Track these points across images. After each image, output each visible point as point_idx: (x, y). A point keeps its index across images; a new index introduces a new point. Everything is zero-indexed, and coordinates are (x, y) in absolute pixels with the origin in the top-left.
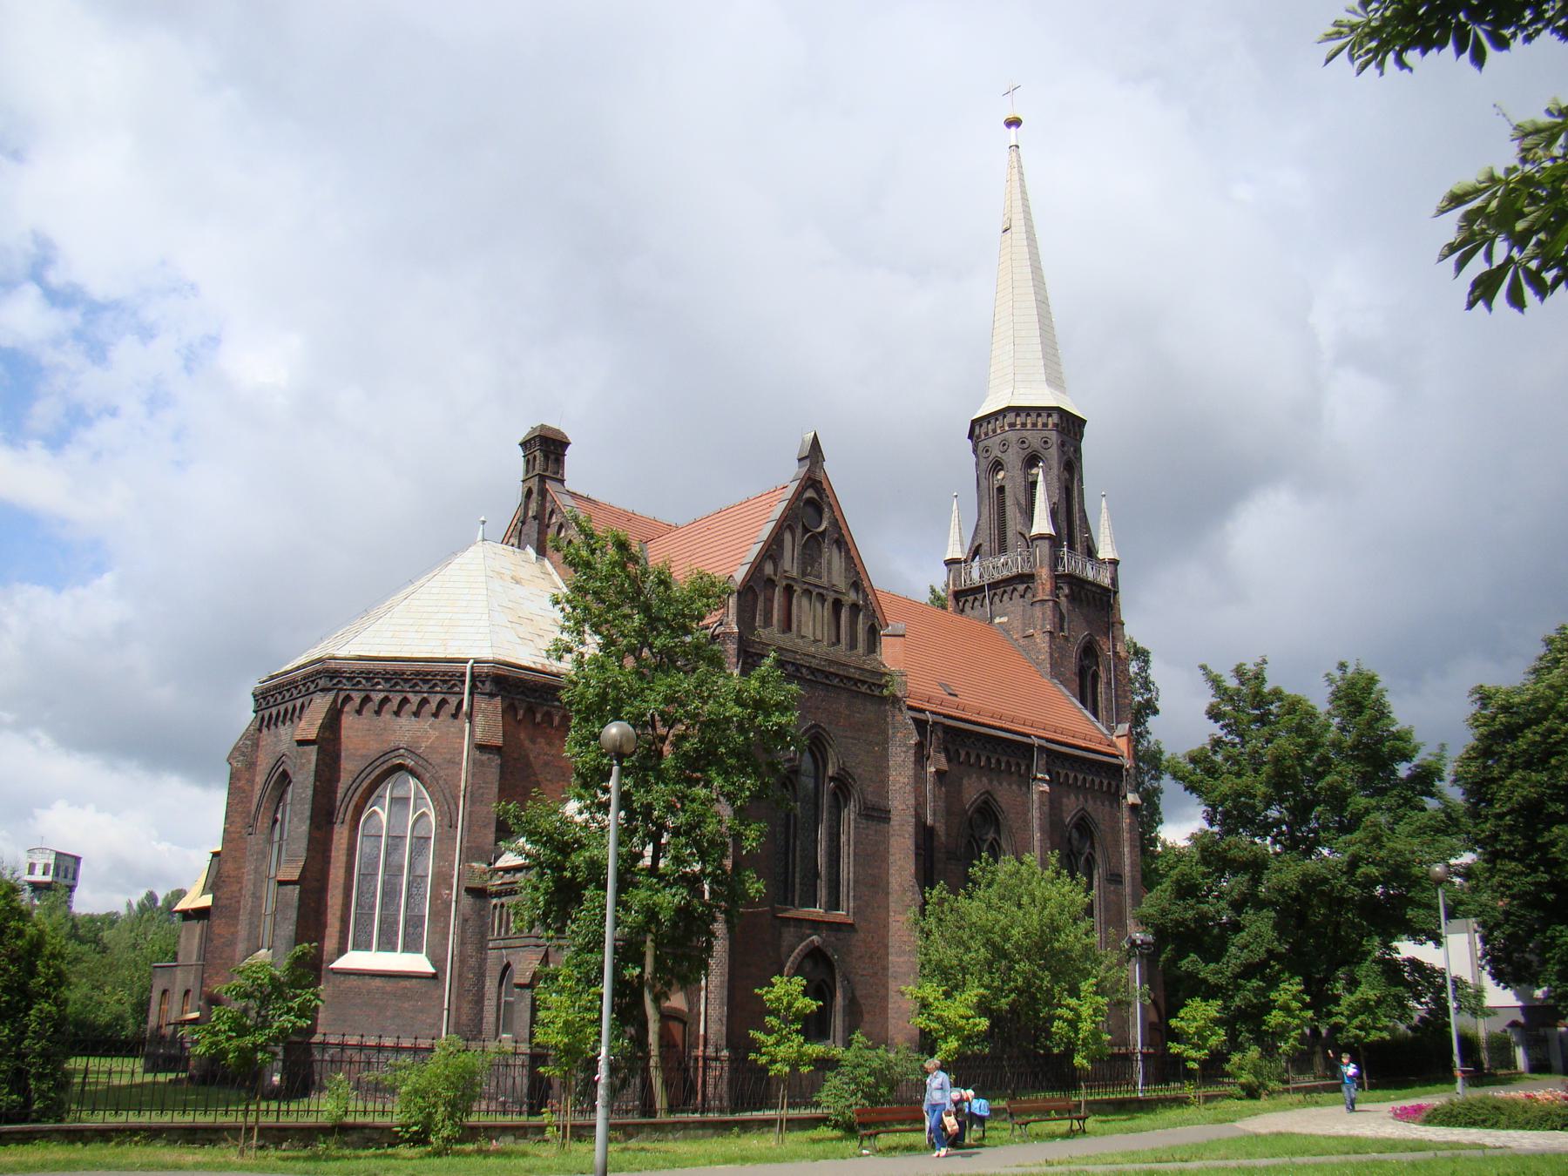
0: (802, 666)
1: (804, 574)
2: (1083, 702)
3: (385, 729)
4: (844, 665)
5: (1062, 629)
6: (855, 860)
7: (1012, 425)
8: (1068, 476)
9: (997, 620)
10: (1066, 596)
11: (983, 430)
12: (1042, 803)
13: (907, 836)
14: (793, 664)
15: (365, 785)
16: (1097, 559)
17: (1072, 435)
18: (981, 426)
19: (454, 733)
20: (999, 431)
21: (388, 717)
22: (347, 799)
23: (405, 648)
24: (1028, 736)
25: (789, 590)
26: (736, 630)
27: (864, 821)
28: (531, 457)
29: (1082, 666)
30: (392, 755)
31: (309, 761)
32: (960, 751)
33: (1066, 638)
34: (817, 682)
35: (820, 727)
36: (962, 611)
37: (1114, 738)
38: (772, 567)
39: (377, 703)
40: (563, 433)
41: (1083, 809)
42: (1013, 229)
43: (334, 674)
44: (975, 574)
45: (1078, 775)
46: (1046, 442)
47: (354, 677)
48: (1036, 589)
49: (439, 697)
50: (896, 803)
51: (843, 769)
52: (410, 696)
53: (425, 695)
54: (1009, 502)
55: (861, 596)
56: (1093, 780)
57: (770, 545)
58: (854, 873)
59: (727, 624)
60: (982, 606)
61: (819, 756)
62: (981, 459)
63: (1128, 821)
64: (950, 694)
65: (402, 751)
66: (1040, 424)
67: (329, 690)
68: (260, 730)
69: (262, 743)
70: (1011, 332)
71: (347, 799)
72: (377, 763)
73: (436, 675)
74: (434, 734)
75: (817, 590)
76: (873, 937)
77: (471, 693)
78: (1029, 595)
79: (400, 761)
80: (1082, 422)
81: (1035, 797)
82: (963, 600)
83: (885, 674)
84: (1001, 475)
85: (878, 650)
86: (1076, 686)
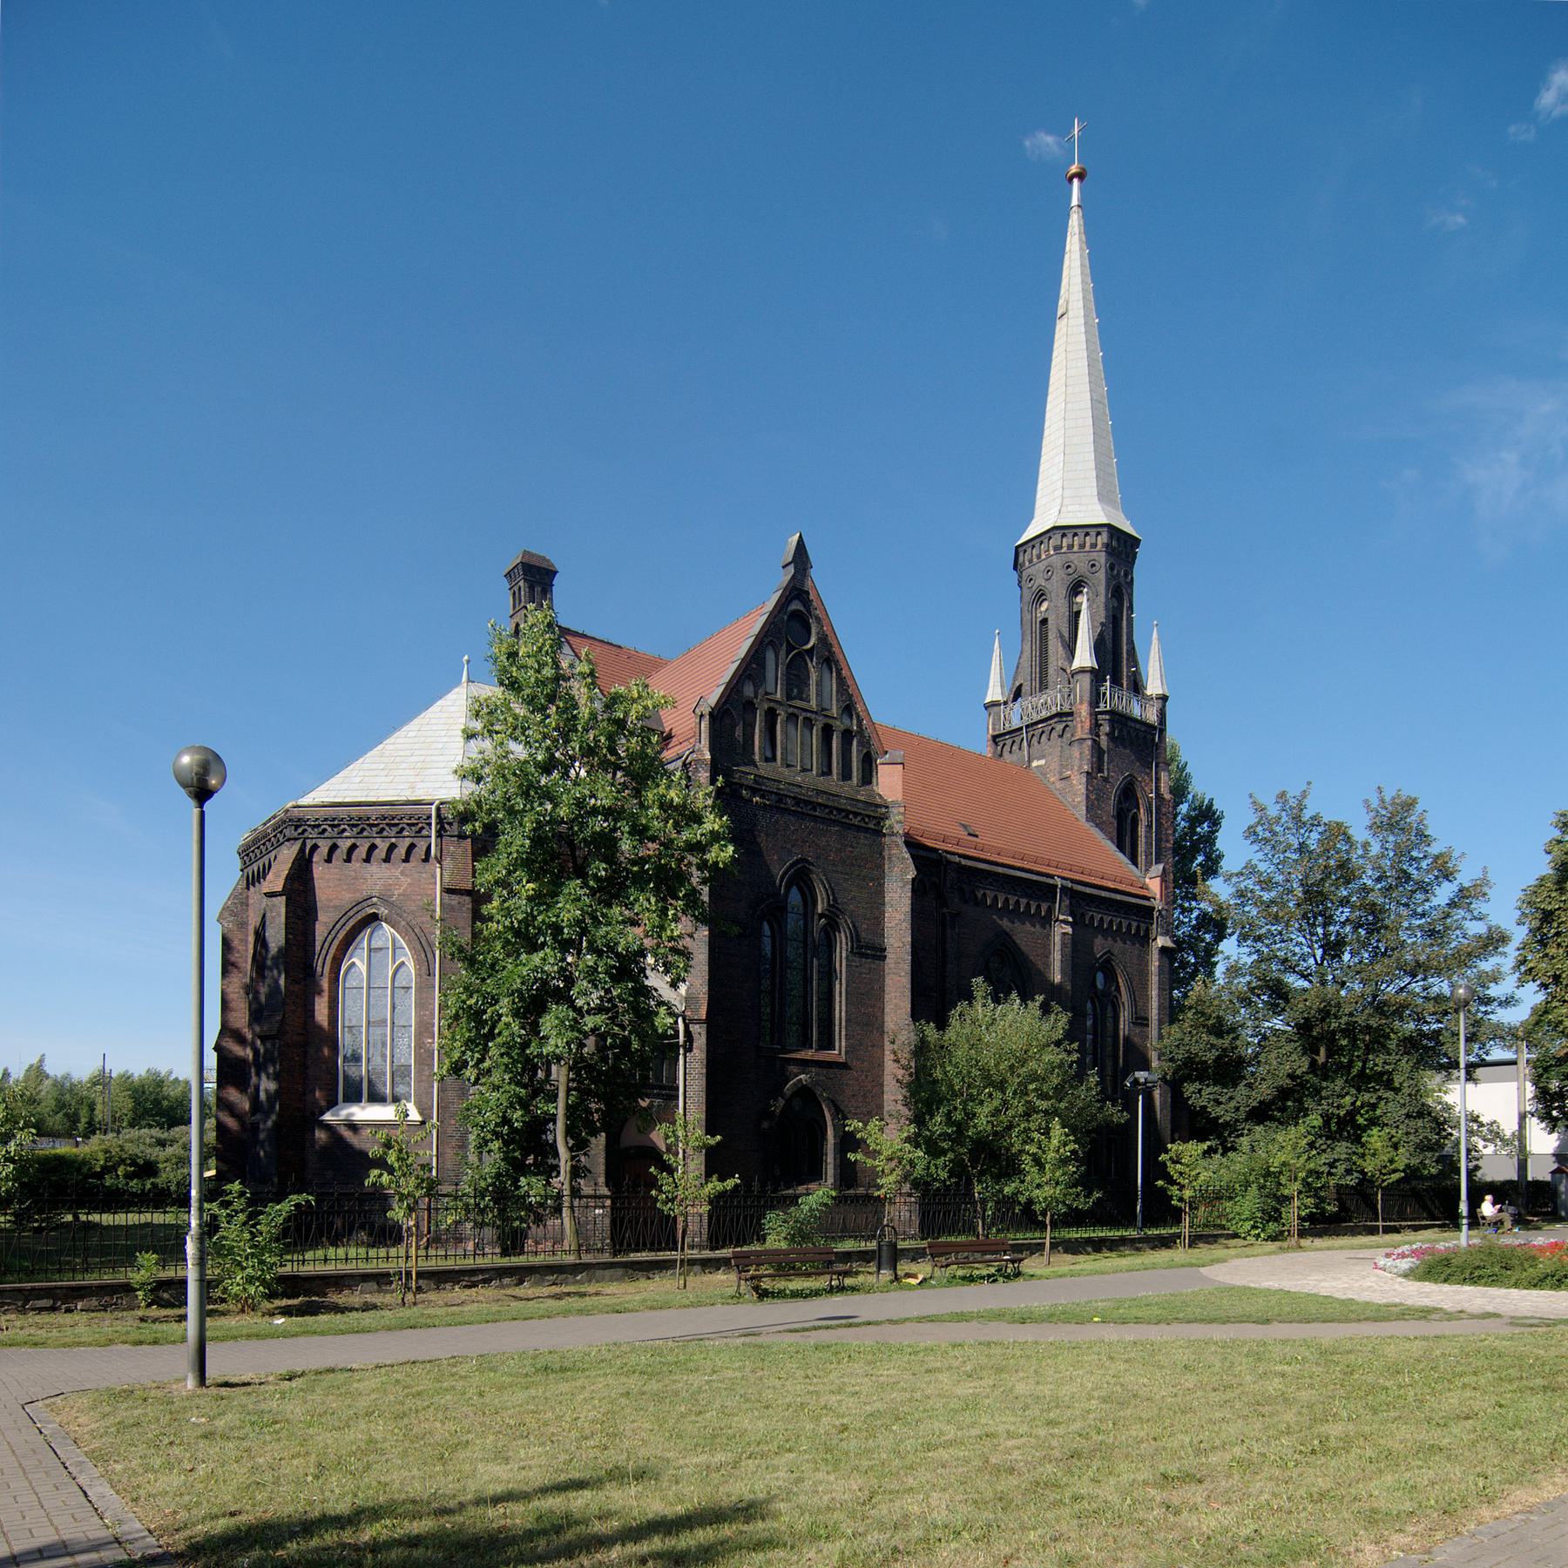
0: (786, 796)
1: (789, 697)
2: (1121, 847)
3: (356, 878)
4: (834, 795)
5: (1100, 770)
6: (847, 998)
7: (1058, 548)
8: (1116, 605)
9: (1035, 764)
10: (1107, 734)
11: (1027, 556)
12: (1063, 944)
13: (903, 974)
14: (776, 794)
15: (341, 936)
16: (1143, 694)
17: (1124, 556)
18: (1025, 551)
19: (425, 879)
20: (1043, 557)
21: (358, 865)
22: (324, 952)
23: (372, 793)
24: (1052, 877)
25: (771, 716)
26: (708, 756)
27: (857, 959)
28: (516, 589)
29: (1121, 809)
30: (364, 904)
31: (279, 915)
32: (999, 897)
33: (1106, 780)
34: (803, 813)
35: (807, 861)
36: (1001, 755)
37: (1147, 880)
38: (752, 687)
39: (345, 851)
40: (548, 561)
41: (1109, 951)
42: (1070, 314)
43: (298, 823)
44: (1015, 717)
45: (1105, 917)
46: (1093, 565)
47: (319, 826)
48: (1075, 727)
49: (408, 842)
50: (892, 941)
51: (833, 906)
52: (378, 841)
53: (393, 840)
54: (1052, 635)
55: (855, 722)
56: (1120, 922)
57: (749, 664)
58: (847, 1012)
59: (698, 750)
60: (1020, 749)
61: (807, 892)
62: (1025, 591)
63: (1157, 964)
64: (970, 834)
65: (375, 899)
66: (1088, 545)
67: (296, 839)
68: (248, 888)
69: (251, 901)
70: (1062, 439)
71: (324, 952)
72: (351, 913)
73: (401, 819)
74: (405, 881)
75: (804, 714)
76: (867, 1076)
77: (439, 835)
78: (1067, 735)
79: (374, 910)
80: (1136, 542)
81: (1058, 939)
82: (1001, 744)
83: (880, 806)
84: (1045, 606)
85: (874, 780)
86: (1113, 830)
